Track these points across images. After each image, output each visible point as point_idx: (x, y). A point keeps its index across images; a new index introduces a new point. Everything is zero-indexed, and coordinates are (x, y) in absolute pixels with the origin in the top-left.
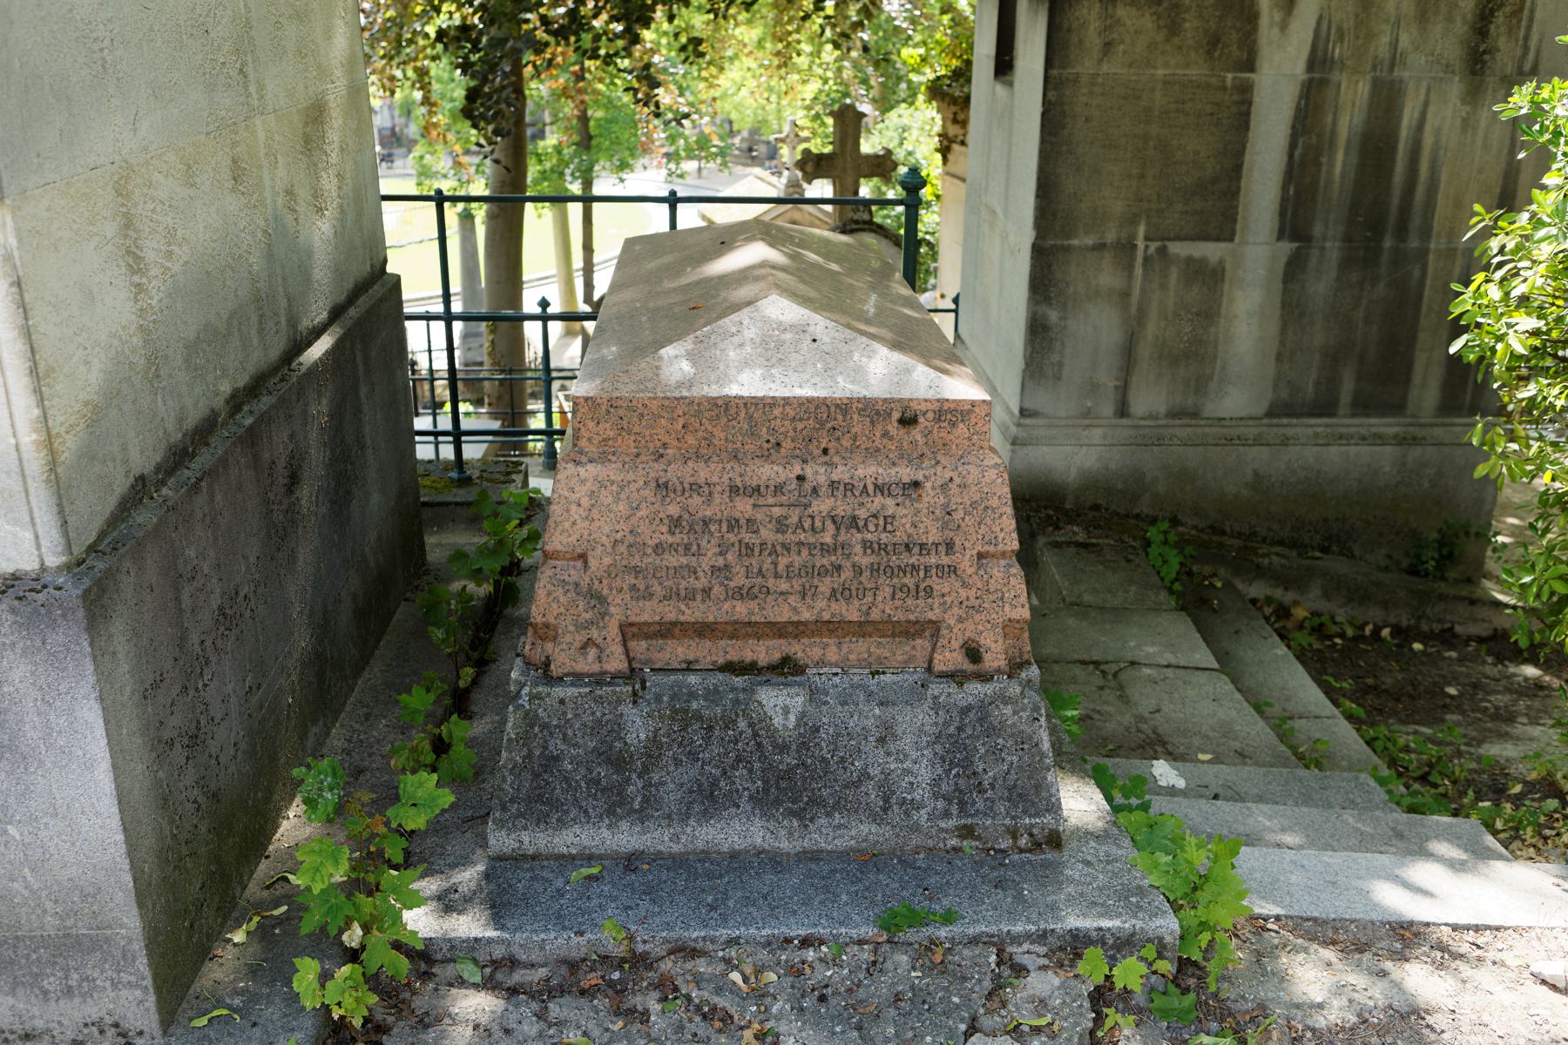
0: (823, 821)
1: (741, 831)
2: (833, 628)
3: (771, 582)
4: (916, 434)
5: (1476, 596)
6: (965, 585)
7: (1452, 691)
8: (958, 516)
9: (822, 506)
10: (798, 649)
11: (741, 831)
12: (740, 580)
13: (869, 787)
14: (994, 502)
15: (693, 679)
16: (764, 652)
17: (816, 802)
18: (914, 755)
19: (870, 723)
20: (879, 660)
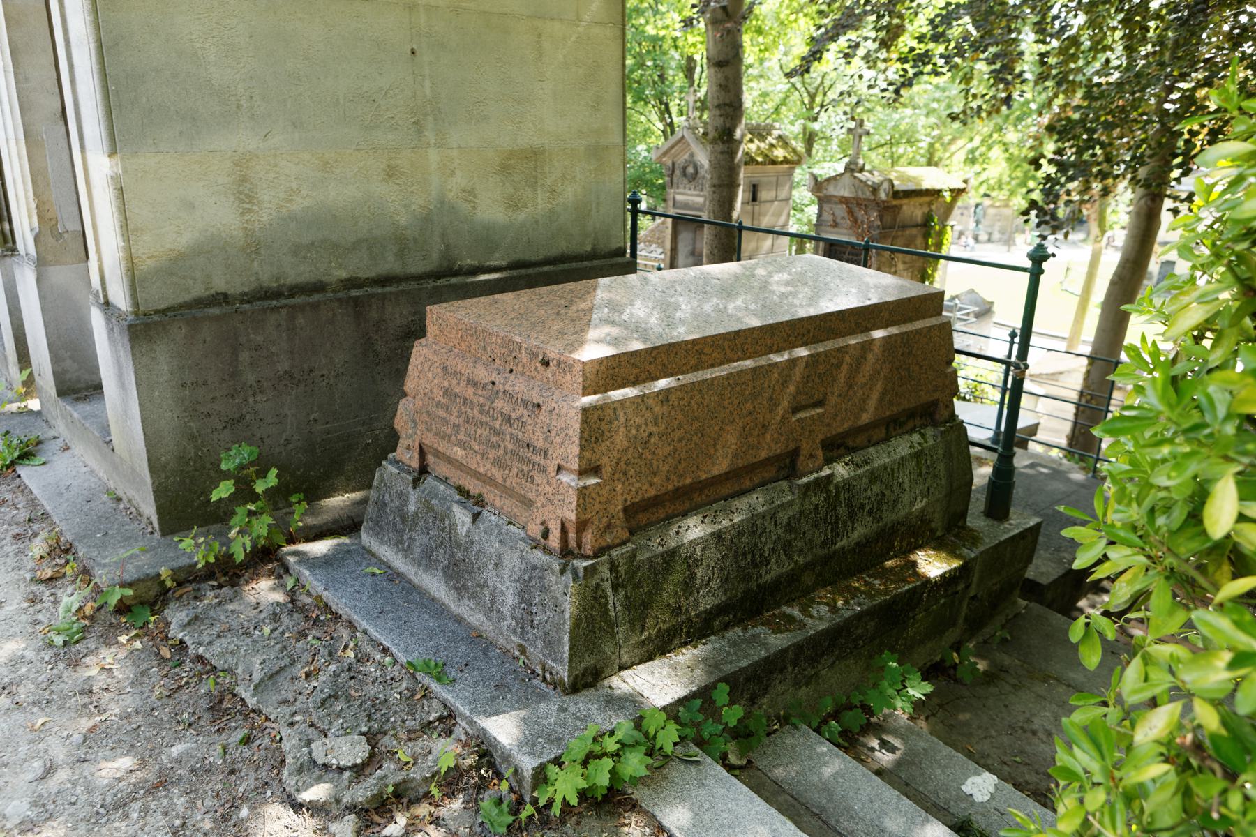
0: (466, 601)
1: (435, 585)
2: (508, 491)
3: (472, 442)
4: (548, 373)
5: (1157, 514)
6: (548, 483)
7: (1138, 18)
8: (553, 434)
9: (499, 404)
10: (490, 495)
11: (435, 585)
12: (461, 436)
13: (487, 591)
14: (571, 433)
15: (442, 487)
16: (473, 486)
17: (465, 587)
18: (508, 583)
19: (493, 550)
20: (516, 516)
